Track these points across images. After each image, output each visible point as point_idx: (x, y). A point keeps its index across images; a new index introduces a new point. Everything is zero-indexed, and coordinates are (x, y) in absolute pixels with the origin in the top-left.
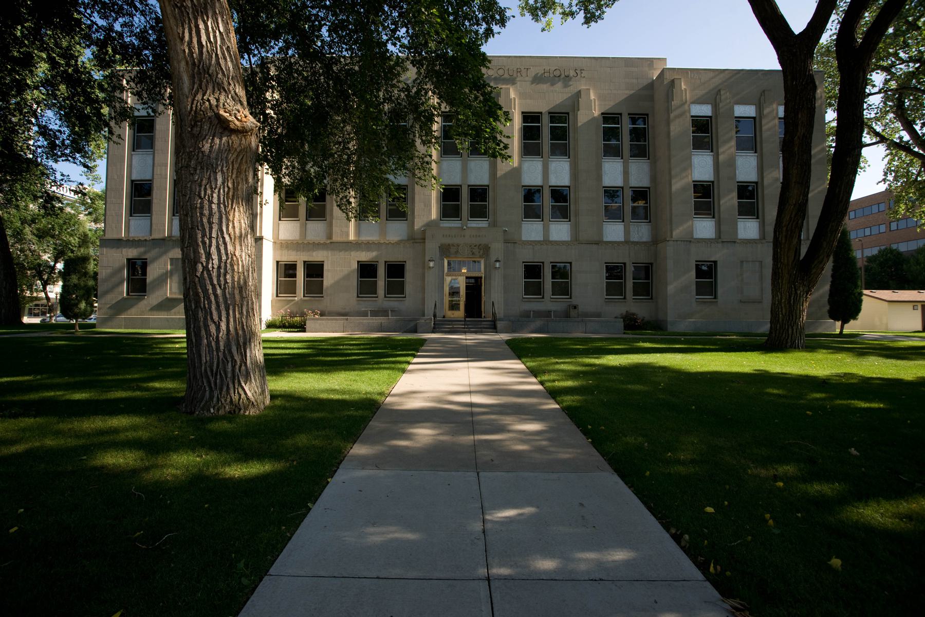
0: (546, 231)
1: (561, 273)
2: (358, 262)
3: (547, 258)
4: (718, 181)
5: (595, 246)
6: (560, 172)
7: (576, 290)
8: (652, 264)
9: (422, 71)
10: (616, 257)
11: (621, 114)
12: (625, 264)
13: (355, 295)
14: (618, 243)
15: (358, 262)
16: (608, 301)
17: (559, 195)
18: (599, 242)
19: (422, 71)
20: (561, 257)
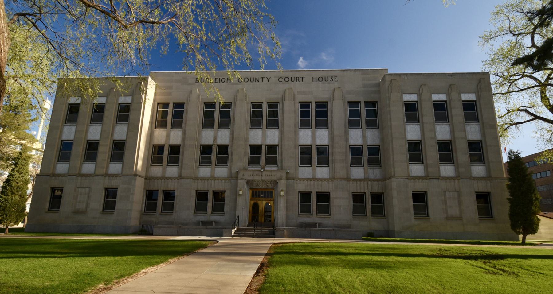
1: (324, 197)
6: (322, 137)
7: (333, 210)
12: (365, 193)
13: (193, 211)
18: (348, 179)
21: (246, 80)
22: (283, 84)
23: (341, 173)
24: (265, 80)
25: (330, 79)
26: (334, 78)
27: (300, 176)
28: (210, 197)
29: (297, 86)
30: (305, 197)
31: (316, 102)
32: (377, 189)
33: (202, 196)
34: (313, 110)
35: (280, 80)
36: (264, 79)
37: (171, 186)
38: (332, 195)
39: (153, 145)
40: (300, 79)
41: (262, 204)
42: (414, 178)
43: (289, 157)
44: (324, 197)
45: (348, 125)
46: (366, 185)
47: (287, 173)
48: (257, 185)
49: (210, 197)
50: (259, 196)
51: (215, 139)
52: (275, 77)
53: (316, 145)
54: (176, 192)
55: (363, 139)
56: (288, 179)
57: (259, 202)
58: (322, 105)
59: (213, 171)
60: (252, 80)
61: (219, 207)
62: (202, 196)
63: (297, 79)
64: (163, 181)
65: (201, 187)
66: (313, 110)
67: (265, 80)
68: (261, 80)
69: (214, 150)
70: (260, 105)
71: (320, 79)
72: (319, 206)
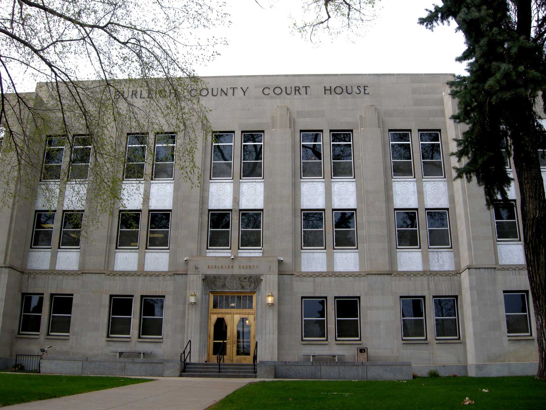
0: (330, 261)
1: (348, 307)
2: (111, 296)
3: (138, 290)
4: (386, 176)
5: (387, 277)
6: (345, 194)
7: (365, 329)
8: (456, 297)
9: (480, 161)
10: (414, 289)
11: (410, 130)
12: (424, 297)
13: (105, 334)
14: (415, 274)
15: (111, 296)
16: (406, 343)
17: (345, 218)
18: (392, 273)
19: (480, 161)
20: (152, 289)
21: (278, 91)
22: (272, 98)
23: (96, 262)
24: (239, 92)
25: (356, 90)
26: (362, 89)
27: (305, 268)
28: (136, 307)
29: (296, 103)
30: (315, 306)
31: (331, 131)
32: (445, 289)
33: (120, 305)
34: (416, 143)
35: (266, 91)
36: (236, 91)
37: (65, 287)
38: (363, 303)
39: (36, 211)
40: (303, 91)
41: (233, 319)
42: (507, 268)
43: (279, 231)
44: (348, 307)
45: (390, 170)
46: (426, 283)
47: (280, 262)
48: (224, 286)
49: (136, 307)
50: (228, 307)
51: (236, 200)
52: (256, 87)
53: (426, 209)
54: (74, 297)
55: (419, 198)
56: (281, 273)
57: (227, 318)
58: (341, 136)
59: (141, 262)
60: (215, 94)
61: (151, 327)
62: (120, 305)
63: (297, 90)
64: (141, 278)
65: (120, 288)
66: (416, 143)
67: (239, 92)
68: (230, 92)
69: (144, 220)
70: (316, 135)
71: (339, 90)
72: (340, 324)
